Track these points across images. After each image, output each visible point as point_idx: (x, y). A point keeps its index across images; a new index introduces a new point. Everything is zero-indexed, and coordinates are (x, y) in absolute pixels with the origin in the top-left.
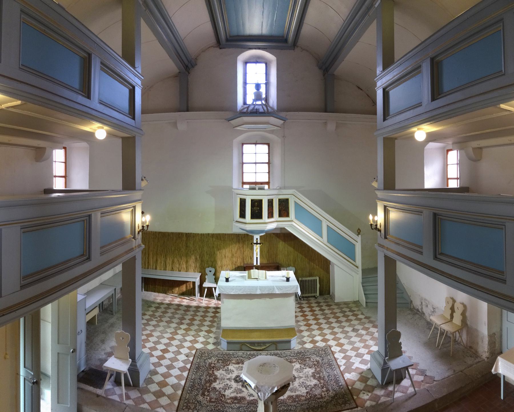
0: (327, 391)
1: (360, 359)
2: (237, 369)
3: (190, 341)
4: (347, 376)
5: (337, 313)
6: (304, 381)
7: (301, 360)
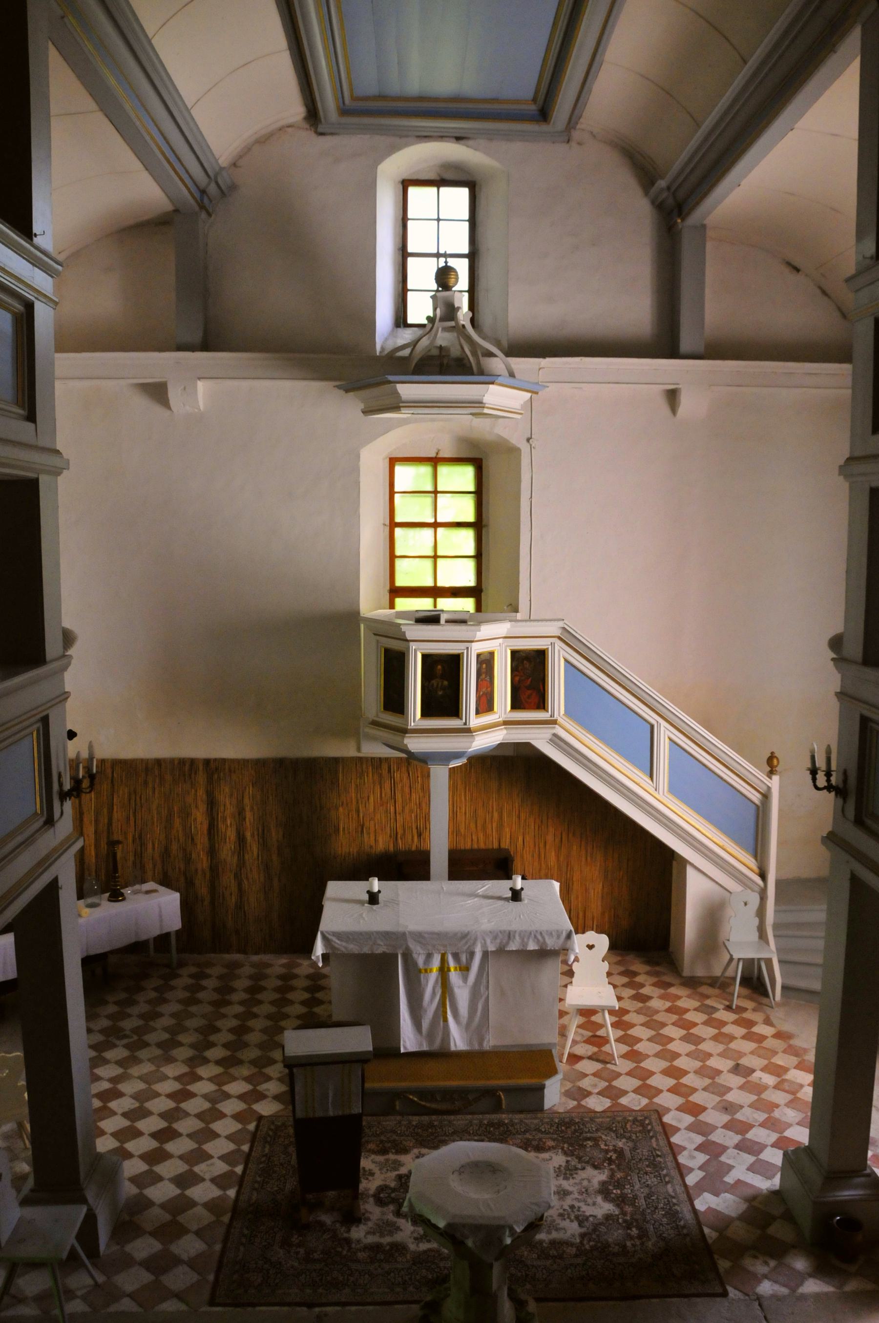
0: (640, 1237)
1: (750, 1159)
2: (382, 1166)
3: (241, 1097)
4: (704, 1202)
5: (687, 1011)
6: (577, 1204)
7: (571, 1145)
